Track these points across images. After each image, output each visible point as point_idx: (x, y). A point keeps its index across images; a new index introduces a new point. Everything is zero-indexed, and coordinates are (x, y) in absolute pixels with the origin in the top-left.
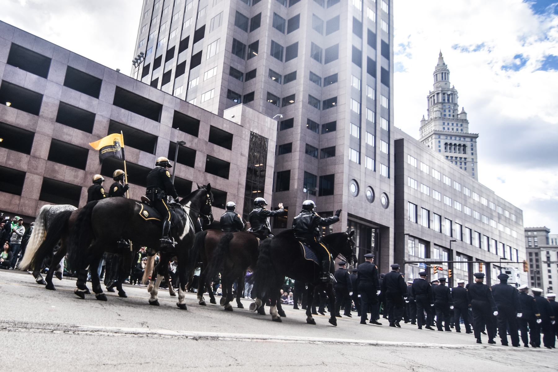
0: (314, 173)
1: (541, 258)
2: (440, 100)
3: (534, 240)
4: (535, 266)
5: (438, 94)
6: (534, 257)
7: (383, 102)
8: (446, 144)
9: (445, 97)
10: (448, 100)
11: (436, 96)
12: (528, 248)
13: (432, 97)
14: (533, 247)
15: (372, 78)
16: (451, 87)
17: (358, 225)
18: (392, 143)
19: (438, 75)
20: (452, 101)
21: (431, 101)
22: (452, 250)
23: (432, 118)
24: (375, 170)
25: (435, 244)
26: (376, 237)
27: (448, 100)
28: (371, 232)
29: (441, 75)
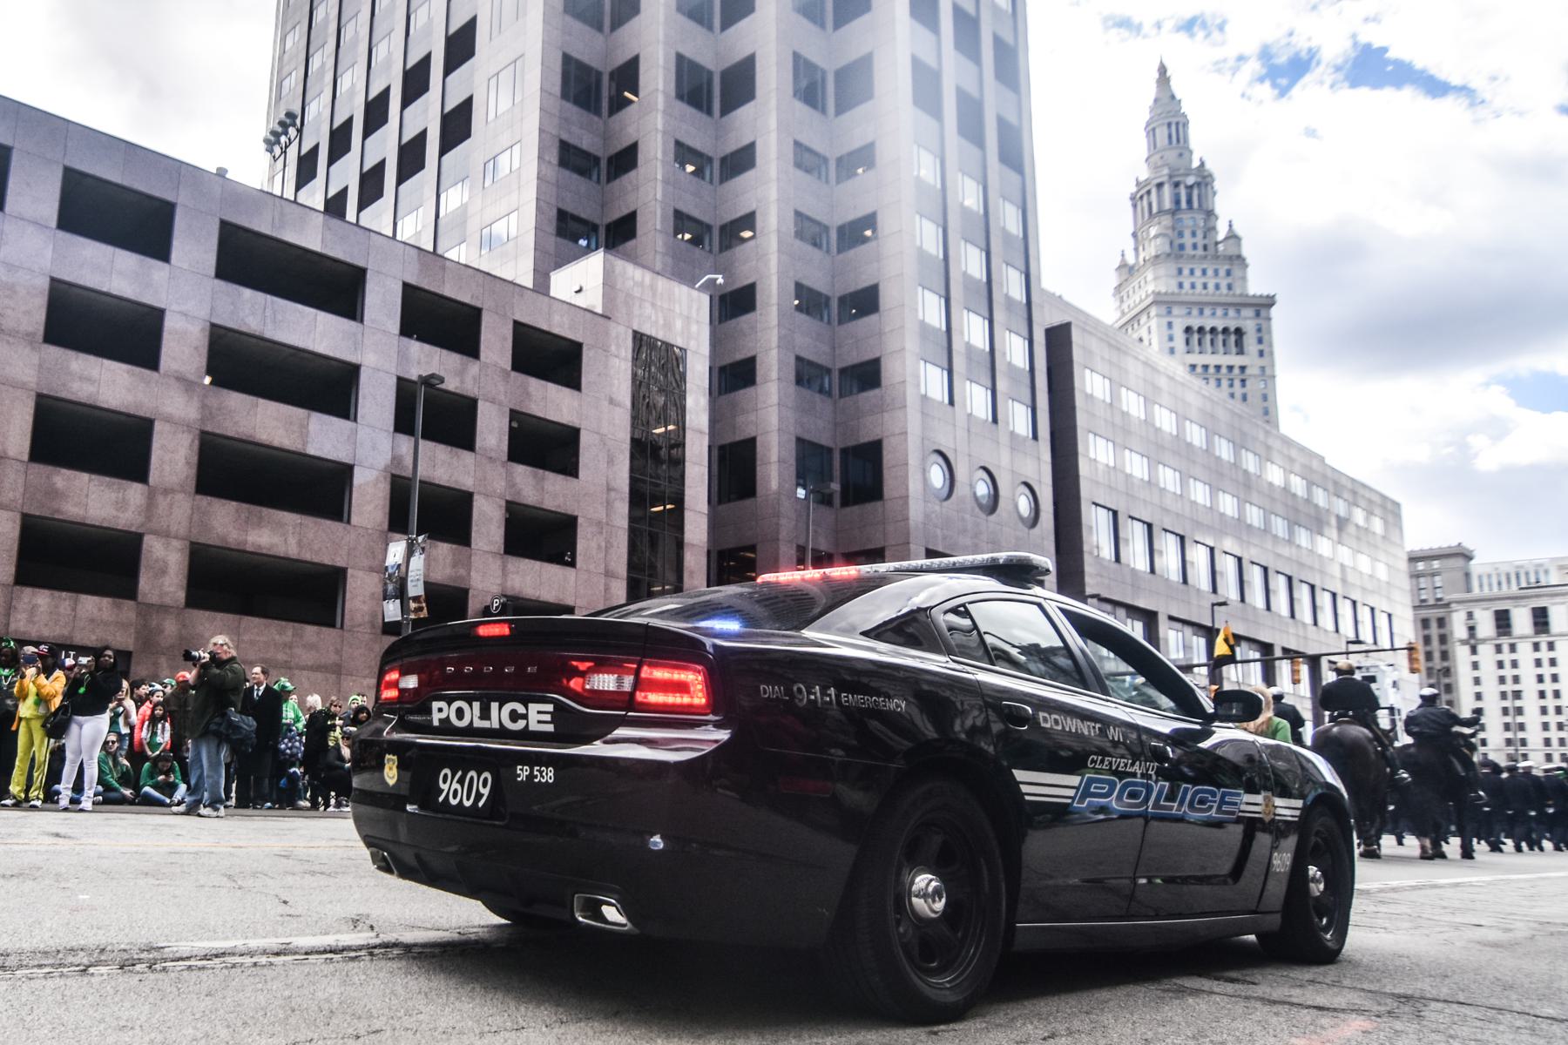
0: (825, 439)
1: (1452, 633)
4: (1437, 655)
5: (1160, 185)
6: (1434, 631)
7: (1009, 219)
8: (1188, 330)
10: (1189, 202)
11: (1154, 191)
12: (1420, 605)
13: (1145, 198)
14: (1431, 602)
23: (1147, 258)
25: (1171, 618)
27: (1189, 202)
29: (1165, 128)
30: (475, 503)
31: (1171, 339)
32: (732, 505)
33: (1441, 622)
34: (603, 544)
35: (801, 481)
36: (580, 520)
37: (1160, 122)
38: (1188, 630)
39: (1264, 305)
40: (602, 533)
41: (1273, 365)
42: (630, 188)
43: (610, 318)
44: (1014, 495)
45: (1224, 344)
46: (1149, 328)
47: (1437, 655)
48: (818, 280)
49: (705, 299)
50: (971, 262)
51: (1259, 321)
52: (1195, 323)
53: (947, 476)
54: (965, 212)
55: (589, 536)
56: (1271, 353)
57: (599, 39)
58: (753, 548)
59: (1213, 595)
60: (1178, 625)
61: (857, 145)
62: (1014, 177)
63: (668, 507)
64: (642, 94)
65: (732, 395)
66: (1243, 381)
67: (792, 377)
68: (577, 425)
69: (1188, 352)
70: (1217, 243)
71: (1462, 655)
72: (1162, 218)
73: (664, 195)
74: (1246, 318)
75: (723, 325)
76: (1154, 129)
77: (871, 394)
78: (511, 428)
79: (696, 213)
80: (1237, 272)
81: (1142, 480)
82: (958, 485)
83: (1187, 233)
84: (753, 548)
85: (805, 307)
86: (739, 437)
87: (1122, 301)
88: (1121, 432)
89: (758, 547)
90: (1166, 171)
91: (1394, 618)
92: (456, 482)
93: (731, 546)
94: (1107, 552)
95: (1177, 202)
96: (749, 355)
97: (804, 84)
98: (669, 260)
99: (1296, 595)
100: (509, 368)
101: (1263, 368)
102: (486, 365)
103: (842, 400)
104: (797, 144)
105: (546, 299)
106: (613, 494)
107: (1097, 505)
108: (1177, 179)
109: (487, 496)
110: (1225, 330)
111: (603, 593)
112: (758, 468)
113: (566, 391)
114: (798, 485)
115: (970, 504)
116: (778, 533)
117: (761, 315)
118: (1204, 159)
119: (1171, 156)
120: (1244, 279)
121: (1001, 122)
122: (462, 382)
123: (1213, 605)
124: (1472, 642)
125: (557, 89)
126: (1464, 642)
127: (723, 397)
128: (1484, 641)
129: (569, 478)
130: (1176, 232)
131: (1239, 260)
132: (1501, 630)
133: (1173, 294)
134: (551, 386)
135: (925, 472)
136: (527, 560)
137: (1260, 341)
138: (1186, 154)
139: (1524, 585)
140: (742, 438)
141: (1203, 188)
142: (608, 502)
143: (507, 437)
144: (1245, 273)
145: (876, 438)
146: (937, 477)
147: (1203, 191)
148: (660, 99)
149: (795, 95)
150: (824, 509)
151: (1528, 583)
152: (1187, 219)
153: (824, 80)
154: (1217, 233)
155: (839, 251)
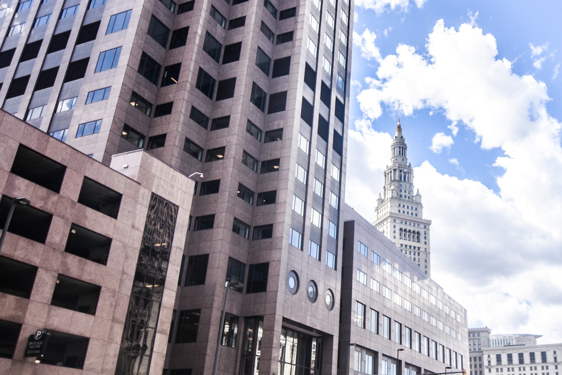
0: (243, 259)
1: (483, 363)
6: (478, 362)
7: (334, 173)
8: (401, 229)
11: (393, 171)
20: (408, 181)
25: (384, 355)
30: (38, 273)
31: (395, 232)
32: (192, 287)
33: (480, 359)
34: (114, 304)
35: (229, 279)
36: (103, 289)
37: (397, 146)
38: (390, 361)
39: (427, 224)
40: (114, 297)
41: (429, 249)
42: (165, 123)
43: (140, 184)
44: (324, 294)
45: (409, 237)
48: (249, 184)
49: (193, 183)
50: (316, 187)
51: (426, 230)
52: (404, 227)
53: (296, 283)
54: (317, 166)
55: (107, 298)
56: (429, 244)
57: (163, 50)
58: (199, 311)
59: (400, 345)
61: (275, 128)
62: (338, 156)
63: (156, 286)
64: (179, 81)
65: (201, 231)
66: (419, 253)
67: (231, 227)
68: (111, 237)
69: (400, 239)
70: (413, 197)
72: (395, 183)
73: (182, 130)
74: (421, 228)
75: (201, 197)
76: (394, 148)
78: (71, 233)
79: (197, 142)
80: (419, 209)
81: (377, 292)
82: (301, 287)
83: (403, 191)
84: (199, 311)
85: (242, 195)
86: (201, 253)
87: (378, 213)
89: (202, 310)
91: (463, 357)
92: (29, 260)
93: (188, 308)
94: (360, 324)
95: (401, 178)
96: (212, 213)
97: (256, 96)
98: (180, 161)
99: (422, 342)
100: (76, 201)
101: (426, 249)
102: (62, 197)
103: (253, 241)
104: (249, 121)
105: (107, 168)
106: (125, 276)
107: (358, 302)
108: (401, 169)
109: (46, 269)
110: (414, 232)
111: (109, 331)
112: (208, 270)
113: (108, 218)
114: (226, 280)
115: (305, 295)
116: (213, 304)
117: (220, 195)
118: (411, 163)
119: (400, 159)
120: (421, 212)
121: (335, 132)
122: (46, 203)
123: (398, 350)
124: (490, 367)
125: (136, 67)
126: (487, 367)
127: (196, 232)
128: (493, 367)
129: (100, 265)
130: (399, 190)
131: (419, 204)
132: (498, 363)
133: (396, 214)
134: (100, 214)
135: (287, 280)
136: (65, 309)
137: (425, 238)
138: (405, 160)
139: (506, 345)
140: (202, 254)
141: (410, 174)
142: (121, 280)
143: (67, 238)
144: (422, 210)
145: (267, 262)
146: (292, 283)
147: (410, 175)
148: (188, 85)
149: (251, 101)
150: (238, 294)
151: (507, 343)
152: (403, 184)
153: (265, 97)
154: (413, 193)
155: (261, 173)
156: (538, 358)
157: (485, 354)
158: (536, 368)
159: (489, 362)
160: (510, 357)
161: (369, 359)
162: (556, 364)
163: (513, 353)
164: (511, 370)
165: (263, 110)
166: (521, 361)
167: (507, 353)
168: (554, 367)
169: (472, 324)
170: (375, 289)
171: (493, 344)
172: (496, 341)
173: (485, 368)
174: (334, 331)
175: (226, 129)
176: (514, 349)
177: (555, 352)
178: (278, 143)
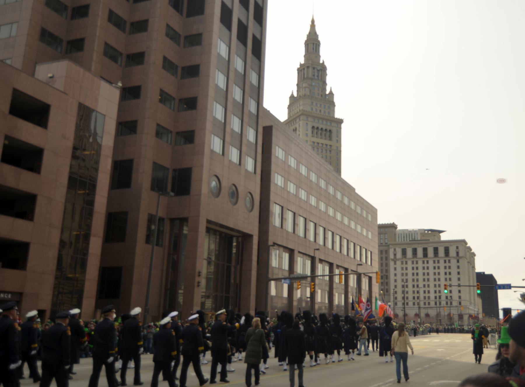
0: (167, 163)
1: (389, 256)
2: (310, 75)
3: (385, 236)
4: (384, 265)
5: (308, 67)
6: (384, 255)
7: (253, 78)
8: (313, 127)
9: (314, 72)
10: (318, 76)
11: (306, 69)
12: (380, 245)
13: (302, 71)
14: (384, 244)
15: (242, 46)
16: (321, 62)
17: (218, 233)
18: (260, 130)
19: (309, 45)
20: (321, 79)
21: (301, 75)
22: (315, 258)
23: (301, 95)
24: (240, 164)
25: (299, 252)
26: (237, 247)
27: (318, 76)
28: (232, 243)
29: (312, 45)
46: (299, 124)
47: (384, 265)
50: (237, 94)
60: (301, 255)
62: (257, 61)
71: (392, 264)
76: (308, 44)
77: (190, 146)
88: (288, 176)
90: (311, 62)
108: (314, 66)
110: (326, 130)
118: (324, 61)
121: (254, 37)
126: (392, 260)
128: (398, 260)
133: (309, 112)
139: (411, 239)
156: (441, 252)
157: (391, 248)
158: (438, 262)
159: (395, 255)
160: (415, 251)
161: (286, 256)
162: (458, 258)
163: (418, 247)
164: (415, 262)
165: (181, 14)
166: (425, 255)
167: (412, 247)
168: (455, 261)
169: (381, 220)
170: (292, 191)
171: (399, 238)
172: (401, 234)
173: (391, 260)
174: (253, 228)
175: (144, 34)
176: (418, 244)
177: (457, 248)
178: (197, 48)
